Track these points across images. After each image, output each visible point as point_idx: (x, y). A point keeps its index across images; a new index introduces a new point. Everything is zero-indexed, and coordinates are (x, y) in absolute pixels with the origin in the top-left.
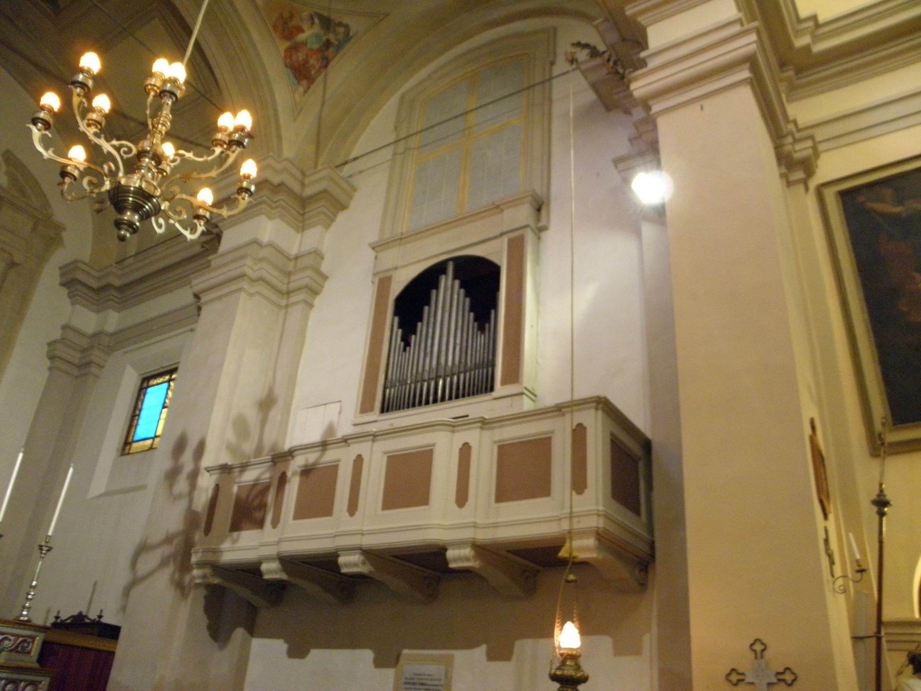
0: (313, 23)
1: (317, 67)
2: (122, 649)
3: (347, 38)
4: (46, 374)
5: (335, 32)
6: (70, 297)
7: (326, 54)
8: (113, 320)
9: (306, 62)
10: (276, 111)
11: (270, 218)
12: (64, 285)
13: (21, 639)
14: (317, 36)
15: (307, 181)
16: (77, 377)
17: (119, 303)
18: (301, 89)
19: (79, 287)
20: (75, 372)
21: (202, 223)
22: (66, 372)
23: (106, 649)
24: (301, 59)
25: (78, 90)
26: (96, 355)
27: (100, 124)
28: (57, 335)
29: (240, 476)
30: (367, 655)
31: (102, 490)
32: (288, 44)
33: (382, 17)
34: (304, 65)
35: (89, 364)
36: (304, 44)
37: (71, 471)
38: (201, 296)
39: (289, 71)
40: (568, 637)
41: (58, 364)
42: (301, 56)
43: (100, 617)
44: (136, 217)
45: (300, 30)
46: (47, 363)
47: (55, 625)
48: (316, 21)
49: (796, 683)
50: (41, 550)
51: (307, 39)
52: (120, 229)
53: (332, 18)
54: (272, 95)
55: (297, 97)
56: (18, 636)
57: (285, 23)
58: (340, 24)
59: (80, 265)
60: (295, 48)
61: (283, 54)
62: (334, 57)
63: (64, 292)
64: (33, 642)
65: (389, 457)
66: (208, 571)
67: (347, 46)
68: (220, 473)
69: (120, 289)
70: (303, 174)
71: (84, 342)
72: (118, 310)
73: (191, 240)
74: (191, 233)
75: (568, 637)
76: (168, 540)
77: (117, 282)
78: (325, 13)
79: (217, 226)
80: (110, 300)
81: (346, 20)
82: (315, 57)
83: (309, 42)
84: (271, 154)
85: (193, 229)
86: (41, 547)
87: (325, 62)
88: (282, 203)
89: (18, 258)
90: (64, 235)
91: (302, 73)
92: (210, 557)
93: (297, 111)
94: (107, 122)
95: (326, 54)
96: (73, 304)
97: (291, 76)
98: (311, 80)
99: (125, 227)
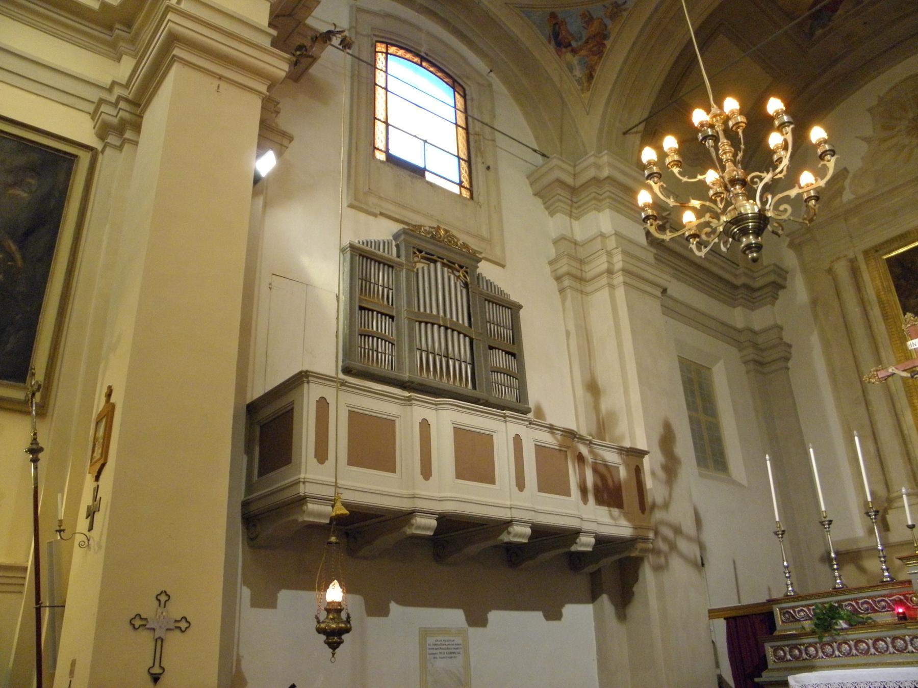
30: (539, 614)
37: (811, 450)
40: (335, 593)
49: (131, 628)
65: (352, 462)
75: (335, 593)
86: (822, 523)
88: (608, 193)
94: (747, 116)
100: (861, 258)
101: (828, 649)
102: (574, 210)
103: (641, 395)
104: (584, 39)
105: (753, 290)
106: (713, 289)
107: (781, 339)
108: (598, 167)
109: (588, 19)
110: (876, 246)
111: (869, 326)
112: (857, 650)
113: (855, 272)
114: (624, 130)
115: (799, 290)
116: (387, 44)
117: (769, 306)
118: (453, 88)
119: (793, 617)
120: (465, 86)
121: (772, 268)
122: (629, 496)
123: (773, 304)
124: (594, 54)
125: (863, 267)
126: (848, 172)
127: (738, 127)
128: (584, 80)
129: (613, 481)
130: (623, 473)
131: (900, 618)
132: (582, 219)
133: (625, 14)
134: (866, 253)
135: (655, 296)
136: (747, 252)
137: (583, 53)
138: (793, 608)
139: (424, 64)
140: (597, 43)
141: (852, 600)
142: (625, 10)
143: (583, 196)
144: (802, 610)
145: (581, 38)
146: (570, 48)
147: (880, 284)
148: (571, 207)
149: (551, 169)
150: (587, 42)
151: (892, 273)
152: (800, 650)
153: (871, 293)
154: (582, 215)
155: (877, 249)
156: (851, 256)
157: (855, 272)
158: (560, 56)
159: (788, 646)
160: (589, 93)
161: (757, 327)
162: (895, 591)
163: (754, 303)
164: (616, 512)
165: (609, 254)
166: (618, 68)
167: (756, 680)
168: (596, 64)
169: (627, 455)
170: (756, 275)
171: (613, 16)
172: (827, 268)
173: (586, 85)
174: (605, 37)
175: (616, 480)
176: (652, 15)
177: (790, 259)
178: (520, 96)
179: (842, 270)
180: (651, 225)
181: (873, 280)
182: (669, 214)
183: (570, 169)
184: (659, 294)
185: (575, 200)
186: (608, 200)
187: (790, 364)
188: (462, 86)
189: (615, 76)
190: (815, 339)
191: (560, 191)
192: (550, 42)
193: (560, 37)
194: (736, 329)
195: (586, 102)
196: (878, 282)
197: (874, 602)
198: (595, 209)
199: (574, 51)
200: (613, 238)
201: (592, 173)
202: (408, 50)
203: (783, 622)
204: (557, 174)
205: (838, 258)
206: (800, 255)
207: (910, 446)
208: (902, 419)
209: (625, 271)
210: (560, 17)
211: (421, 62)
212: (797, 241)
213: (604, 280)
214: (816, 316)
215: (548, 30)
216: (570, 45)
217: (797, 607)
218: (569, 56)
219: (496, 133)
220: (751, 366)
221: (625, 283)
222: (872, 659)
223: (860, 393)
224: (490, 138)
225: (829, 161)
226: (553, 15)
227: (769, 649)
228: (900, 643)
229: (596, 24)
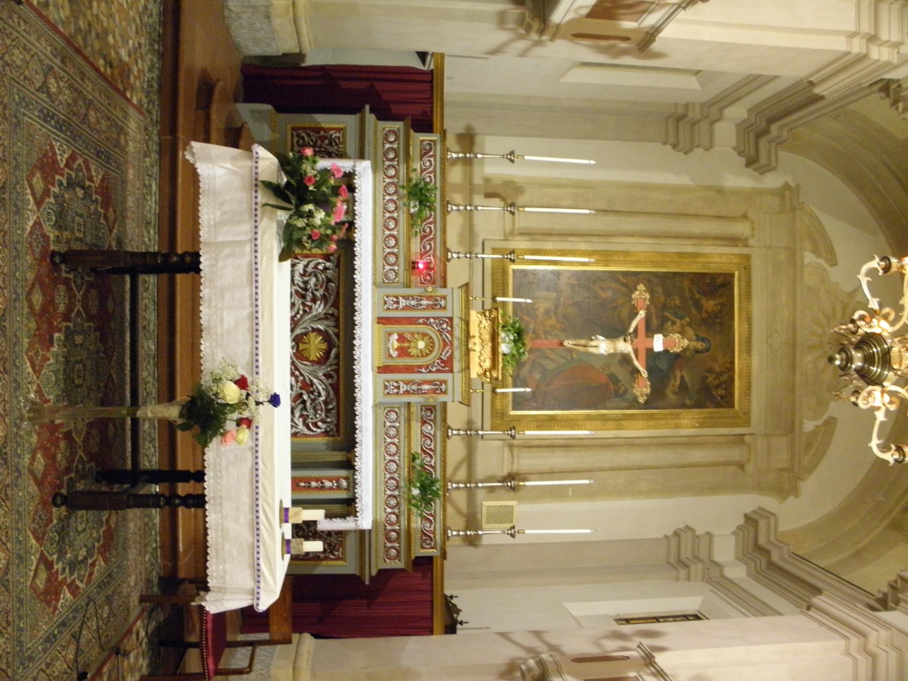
2: (437, 641)
4: (660, 536)
6: (738, 528)
8: (737, 572)
12: (746, 516)
13: (432, 536)
16: (669, 563)
17: (756, 571)
19: (752, 529)
20: (672, 561)
21: (897, 456)
22: (668, 550)
23: (435, 627)
26: (697, 569)
28: (700, 531)
29: (648, 674)
31: (575, 614)
35: (687, 566)
38: (812, 609)
41: (674, 541)
43: (461, 623)
44: (860, 364)
46: (670, 533)
47: (446, 596)
50: (511, 529)
52: (839, 353)
56: (434, 533)
59: (772, 519)
63: (741, 521)
64: (432, 548)
66: (537, 671)
68: (642, 657)
69: (771, 565)
71: (703, 555)
72: (749, 574)
73: (871, 448)
76: (553, 648)
77: (775, 558)
80: (755, 561)
85: (885, 448)
89: (750, 468)
90: (792, 498)
92: (551, 668)
96: (734, 533)
99: (844, 355)
100: (745, 251)
101: (392, 189)
103: (708, 42)
105: (759, 135)
106: (779, 102)
107: (698, 146)
110: (750, 269)
111: (677, 236)
112: (389, 218)
113: (733, 241)
115: (739, 179)
117: (734, 143)
119: (425, 154)
121: (773, 164)
122: (600, 26)
123: (734, 149)
125: (736, 250)
126: (831, 266)
129: (624, 14)
130: (628, 24)
131: (414, 263)
134: (747, 258)
135: (812, 75)
138: (434, 156)
141: (435, 218)
144: (431, 164)
147: (713, 260)
151: (720, 275)
152: (392, 160)
153: (708, 249)
155: (747, 269)
156: (751, 242)
157: (733, 241)
159: (398, 147)
161: (718, 126)
162: (438, 262)
163: (746, 129)
164: (585, 12)
167: (367, 107)
169: (647, 33)
170: (773, 144)
172: (749, 215)
175: (623, 17)
177: (772, 181)
179: (740, 229)
181: (721, 255)
182: (897, 109)
184: (812, 79)
187: (668, 148)
190: (684, 180)
194: (726, 107)
196: (716, 259)
197: (430, 240)
203: (422, 141)
205: (753, 229)
206: (772, 192)
207: (557, 238)
208: (583, 239)
209: (865, 56)
212: (787, 193)
213: (866, 28)
214: (708, 188)
217: (435, 161)
220: (680, 111)
221: (848, 53)
222: (379, 233)
223: (618, 208)
225: (892, 455)
227: (397, 125)
228: (392, 259)
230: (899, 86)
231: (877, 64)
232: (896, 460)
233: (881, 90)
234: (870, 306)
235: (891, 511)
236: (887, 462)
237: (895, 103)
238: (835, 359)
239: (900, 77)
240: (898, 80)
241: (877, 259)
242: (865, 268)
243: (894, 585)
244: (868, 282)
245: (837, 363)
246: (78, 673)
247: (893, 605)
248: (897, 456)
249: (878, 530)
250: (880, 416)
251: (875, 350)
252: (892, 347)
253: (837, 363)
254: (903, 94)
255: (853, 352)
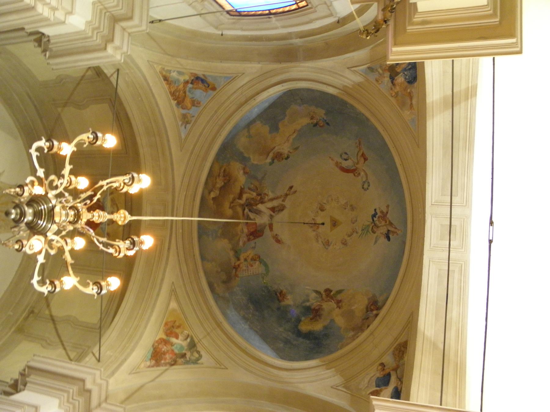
0: (186, 339)
1: (167, 361)
3: (196, 362)
5: (192, 354)
7: (178, 359)
9: (164, 353)
10: (125, 360)
11: (60, 406)
14: (182, 347)
15: (104, 405)
18: (148, 363)
21: (50, 288)
24: (163, 350)
25: (91, 137)
27: (70, 185)
32: (164, 337)
33: (223, 367)
34: (162, 354)
36: (172, 344)
39: (152, 349)
42: (164, 348)
45: (177, 337)
48: (189, 340)
51: (175, 344)
52: (14, 208)
53: (197, 345)
54: (132, 350)
55: (142, 365)
57: (173, 327)
58: (198, 352)
60: (166, 342)
61: (157, 339)
62: (180, 365)
67: (192, 366)
70: (106, 398)
73: (32, 285)
74: (38, 282)
78: (196, 341)
79: (25, 385)
81: (203, 353)
82: (171, 356)
83: (175, 346)
84: (102, 369)
85: (42, 282)
87: (173, 363)
88: (77, 403)
91: (157, 356)
93: (135, 371)
95: (178, 359)
97: (151, 352)
98: (158, 364)
102: (102, 7)
104: (187, 93)
108: (117, 48)
109: (195, 103)
114: (120, 72)
116: (299, 8)
118: (239, 12)
120: (232, 17)
124: (176, 91)
127: (116, 251)
128: (168, 74)
132: (91, 7)
133: (180, 123)
136: (19, 211)
137: (181, 86)
139: (267, 12)
140: (179, 98)
142: (182, 125)
143: (106, 21)
145: (189, 91)
146: (190, 82)
148: (105, 8)
149: (141, 21)
150: (185, 92)
154: (93, 8)
158: (192, 73)
160: (158, 72)
165: (54, 9)
166: (156, 96)
168: (170, 88)
171: (184, 116)
173: (164, 73)
174: (178, 104)
176: (167, 137)
178: (194, 34)
180: (88, 138)
182: (45, 55)
183: (130, 31)
185: (107, 14)
186: (90, 34)
188: (234, 16)
189: (154, 92)
191: (123, 12)
192: (204, 75)
193: (200, 82)
195: (155, 66)
198: (91, 22)
199: (187, 82)
200: (62, 18)
201: (117, 42)
202: (284, 12)
204: (136, 21)
209: (33, 8)
210: (210, 92)
211: (270, 12)
215: (210, 80)
216: (192, 83)
218: (187, 78)
219: (196, 13)
224: (194, 4)
225: (47, 288)
226: (214, 89)
229: (189, 105)
230: (49, 41)
231: (39, 17)
232: (49, 292)
233: (35, 40)
234: (38, 174)
235: (17, 320)
236: (44, 294)
237: (44, 51)
238: (11, 214)
239: (50, 34)
240: (48, 36)
241: (44, 140)
242: (36, 145)
243: (23, 372)
244: (37, 156)
245: (13, 216)
246: (30, 194)
247: (22, 387)
248: (50, 288)
249: (10, 334)
250: (41, 259)
251: (42, 207)
252: (55, 206)
253: (13, 216)
254: (50, 46)
255: (26, 208)
